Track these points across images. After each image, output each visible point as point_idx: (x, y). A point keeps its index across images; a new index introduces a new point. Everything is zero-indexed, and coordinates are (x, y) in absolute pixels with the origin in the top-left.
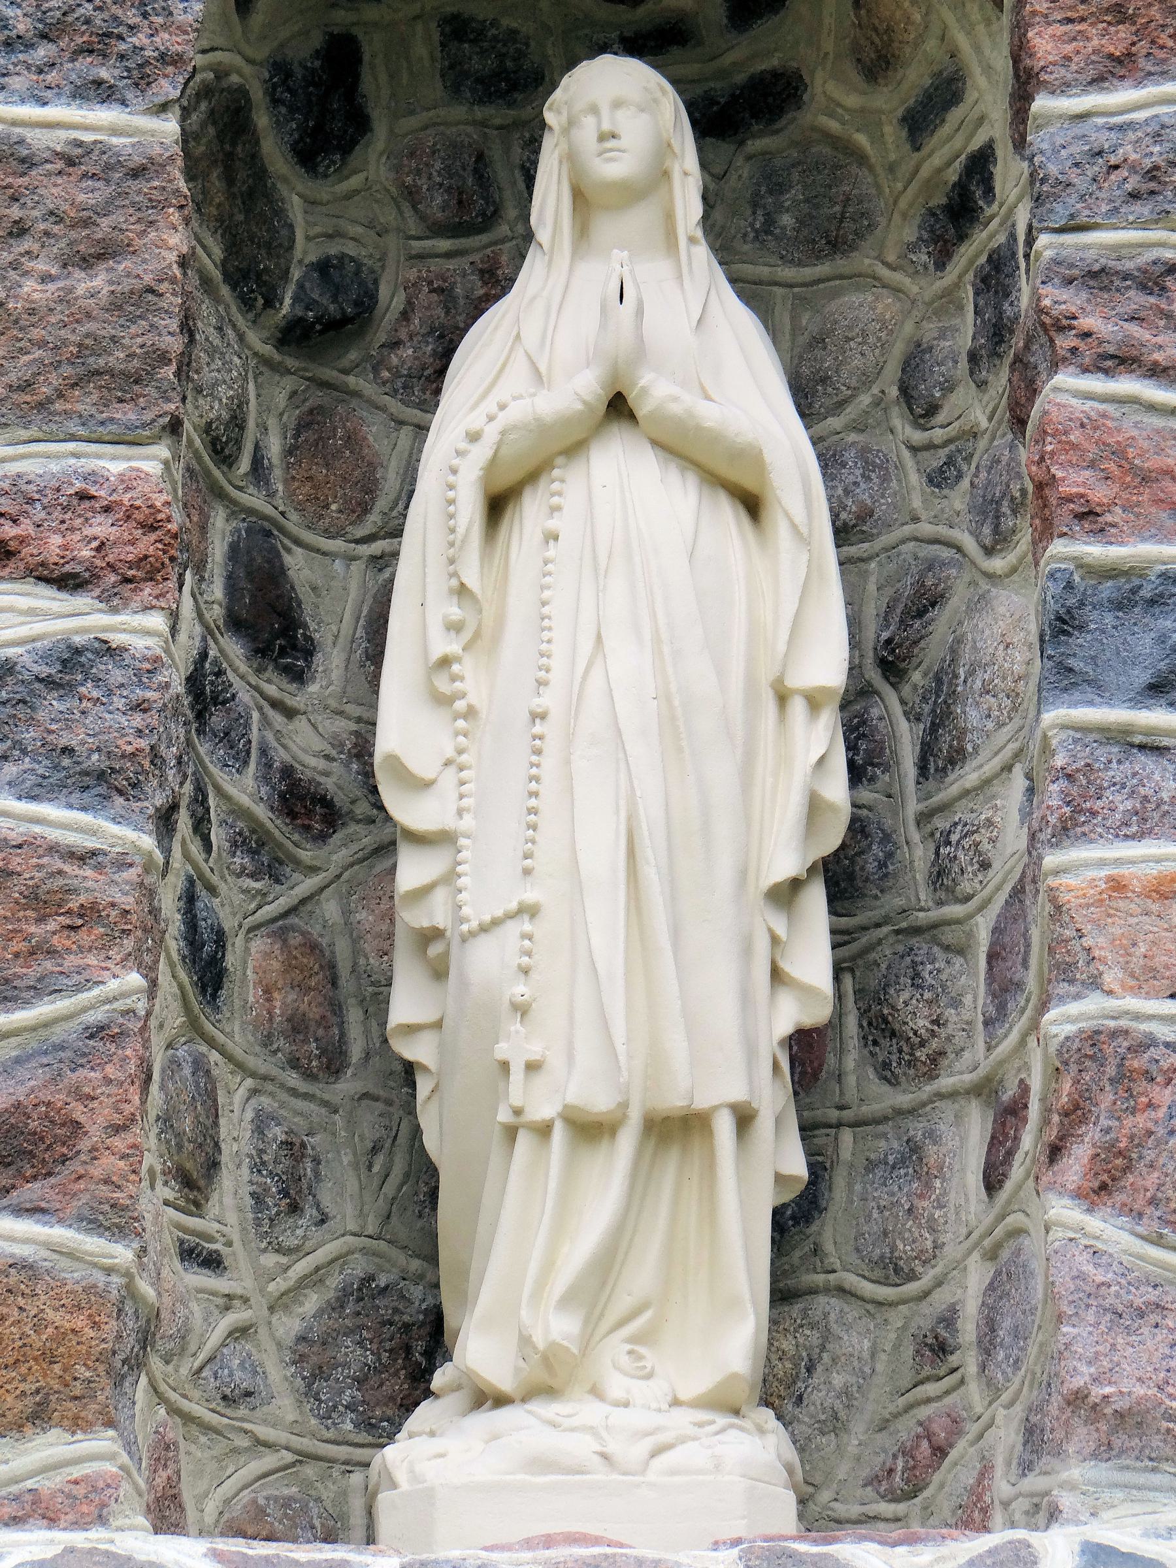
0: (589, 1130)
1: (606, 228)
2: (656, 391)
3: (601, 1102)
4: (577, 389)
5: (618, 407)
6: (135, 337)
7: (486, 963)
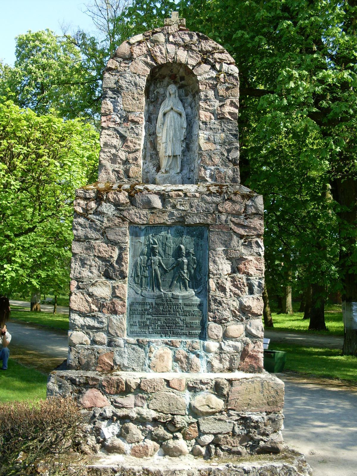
3: (170, 155)
4: (169, 108)
5: (172, 109)
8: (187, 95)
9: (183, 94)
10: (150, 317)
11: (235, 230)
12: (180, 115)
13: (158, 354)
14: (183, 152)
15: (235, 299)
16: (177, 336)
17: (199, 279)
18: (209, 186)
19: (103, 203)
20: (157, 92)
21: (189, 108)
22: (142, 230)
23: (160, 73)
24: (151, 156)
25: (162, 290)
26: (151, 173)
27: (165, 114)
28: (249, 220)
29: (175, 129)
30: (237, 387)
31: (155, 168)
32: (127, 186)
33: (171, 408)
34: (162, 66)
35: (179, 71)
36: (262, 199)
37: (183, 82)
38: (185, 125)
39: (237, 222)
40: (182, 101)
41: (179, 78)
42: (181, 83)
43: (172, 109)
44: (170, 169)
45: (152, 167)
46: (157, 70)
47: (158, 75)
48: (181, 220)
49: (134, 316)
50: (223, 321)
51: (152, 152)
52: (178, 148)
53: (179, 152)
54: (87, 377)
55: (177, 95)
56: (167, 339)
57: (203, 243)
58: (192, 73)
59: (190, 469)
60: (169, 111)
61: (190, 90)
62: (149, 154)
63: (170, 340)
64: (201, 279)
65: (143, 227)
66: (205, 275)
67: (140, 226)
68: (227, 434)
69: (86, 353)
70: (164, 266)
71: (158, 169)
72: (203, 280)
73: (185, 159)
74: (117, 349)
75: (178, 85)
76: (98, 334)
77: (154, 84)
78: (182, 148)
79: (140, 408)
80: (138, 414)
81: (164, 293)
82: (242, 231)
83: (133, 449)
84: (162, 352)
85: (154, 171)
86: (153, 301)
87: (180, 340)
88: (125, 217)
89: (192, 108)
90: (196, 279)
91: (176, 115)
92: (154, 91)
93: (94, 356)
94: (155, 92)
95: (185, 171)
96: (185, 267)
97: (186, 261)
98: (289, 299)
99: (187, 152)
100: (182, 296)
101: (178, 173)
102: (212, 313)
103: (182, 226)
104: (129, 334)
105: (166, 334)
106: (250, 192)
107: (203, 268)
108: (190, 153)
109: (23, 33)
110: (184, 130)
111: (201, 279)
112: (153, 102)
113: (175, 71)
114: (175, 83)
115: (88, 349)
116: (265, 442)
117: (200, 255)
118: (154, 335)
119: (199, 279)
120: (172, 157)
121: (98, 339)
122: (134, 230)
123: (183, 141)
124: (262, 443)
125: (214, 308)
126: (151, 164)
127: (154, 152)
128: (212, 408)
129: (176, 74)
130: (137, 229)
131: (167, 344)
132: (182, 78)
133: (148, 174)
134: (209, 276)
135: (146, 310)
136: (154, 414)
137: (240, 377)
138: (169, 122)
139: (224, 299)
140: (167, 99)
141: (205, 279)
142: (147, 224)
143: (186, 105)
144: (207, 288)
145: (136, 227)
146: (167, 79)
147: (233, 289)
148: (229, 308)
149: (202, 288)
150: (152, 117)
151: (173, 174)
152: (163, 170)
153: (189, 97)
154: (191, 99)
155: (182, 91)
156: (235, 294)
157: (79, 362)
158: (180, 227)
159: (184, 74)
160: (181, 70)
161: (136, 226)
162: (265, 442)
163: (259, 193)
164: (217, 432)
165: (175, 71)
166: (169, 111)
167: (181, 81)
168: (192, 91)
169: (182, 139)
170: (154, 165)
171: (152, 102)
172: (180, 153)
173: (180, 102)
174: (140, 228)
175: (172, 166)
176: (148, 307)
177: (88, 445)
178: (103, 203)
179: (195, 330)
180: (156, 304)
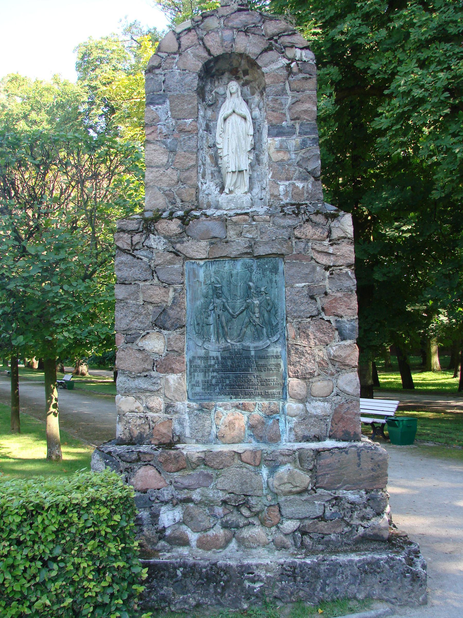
0: (233, 172)
1: (235, 96)
2: (237, 111)
3: (234, 170)
4: (230, 111)
5: (234, 112)
6: (193, 111)
7: (225, 159)
8: (253, 94)
9: (249, 92)
10: (215, 374)
11: (317, 260)
12: (245, 118)
13: (227, 421)
14: (251, 165)
15: (322, 347)
16: (250, 398)
17: (274, 324)
18: (284, 207)
19: (151, 236)
20: (216, 93)
21: (257, 109)
22: (201, 267)
23: (217, 67)
24: (212, 173)
25: (229, 341)
26: (213, 195)
27: (225, 120)
28: (335, 246)
29: (239, 138)
30: (327, 460)
31: (218, 189)
32: (180, 213)
33: (243, 487)
34: (217, 59)
35: (240, 64)
36: (350, 219)
37: (247, 77)
38: (251, 132)
39: (320, 249)
40: (247, 102)
41: (241, 72)
42: (244, 78)
43: (234, 112)
44: (235, 188)
45: (214, 187)
46: (212, 64)
47: (214, 71)
48: (249, 251)
49: (196, 374)
50: (308, 376)
51: (213, 169)
52: (244, 161)
53: (245, 166)
54: (140, 452)
55: (240, 94)
56: (236, 401)
57: (278, 279)
58: (256, 64)
59: (269, 563)
60: (231, 115)
61: (257, 87)
62: (210, 172)
63: (241, 402)
64: (277, 324)
65: (202, 263)
66: (282, 319)
67: (198, 261)
68: (316, 518)
69: (139, 422)
70: (231, 311)
71: (222, 189)
72: (280, 326)
73: (255, 175)
74: (176, 416)
75: (242, 82)
76: (152, 398)
77: (211, 83)
78: (250, 161)
79: (205, 489)
80: (202, 495)
81: (232, 344)
82: (324, 260)
83: (199, 540)
84: (231, 418)
85: (217, 192)
86: (219, 354)
87: (255, 402)
88: (178, 251)
89: (260, 110)
90: (271, 324)
91: (239, 119)
92: (211, 91)
93: (148, 426)
94: (213, 93)
95: (256, 190)
96: (257, 310)
97: (257, 302)
98: (434, 348)
99: (257, 166)
100: (254, 347)
101: (246, 193)
102: (292, 367)
103: (250, 258)
104: (190, 397)
105: (237, 395)
106: (336, 210)
107: (279, 310)
108: (261, 167)
109: (82, 39)
110: (251, 138)
111: (277, 324)
112: (212, 105)
113: (235, 63)
114: (238, 79)
115: (140, 418)
116: (365, 527)
117: (275, 294)
118: (223, 396)
119: (274, 324)
120: (237, 173)
121: (151, 405)
122: (191, 266)
123: (250, 152)
124: (361, 530)
125: (295, 360)
126: (212, 183)
127: (215, 169)
128: (296, 487)
129: (237, 68)
130: (195, 266)
131: (237, 407)
132: (246, 73)
133: (210, 197)
134: (287, 319)
135: (210, 366)
136: (222, 496)
137: (330, 447)
138: (230, 129)
139: (307, 349)
140: (227, 101)
141: (283, 324)
142: (206, 259)
143: (253, 106)
144: (286, 335)
145: (193, 263)
146: (227, 75)
147: (318, 335)
148: (314, 360)
149: (279, 336)
150: (211, 124)
151: (239, 194)
152: (226, 190)
153: (256, 96)
154: (259, 98)
155: (247, 89)
156: (320, 341)
157: (130, 434)
158: (247, 260)
159: (247, 67)
160: (243, 62)
161: (193, 261)
162: (365, 527)
163: (347, 211)
164: (304, 516)
165: (235, 63)
166: (231, 115)
167: (244, 76)
168: (259, 88)
169: (249, 149)
170: (217, 185)
171: (210, 106)
172: (248, 168)
173: (244, 103)
174: (199, 264)
175: (238, 184)
176: (213, 362)
177: (143, 535)
178: (151, 236)
179: (273, 388)
180: (222, 358)
